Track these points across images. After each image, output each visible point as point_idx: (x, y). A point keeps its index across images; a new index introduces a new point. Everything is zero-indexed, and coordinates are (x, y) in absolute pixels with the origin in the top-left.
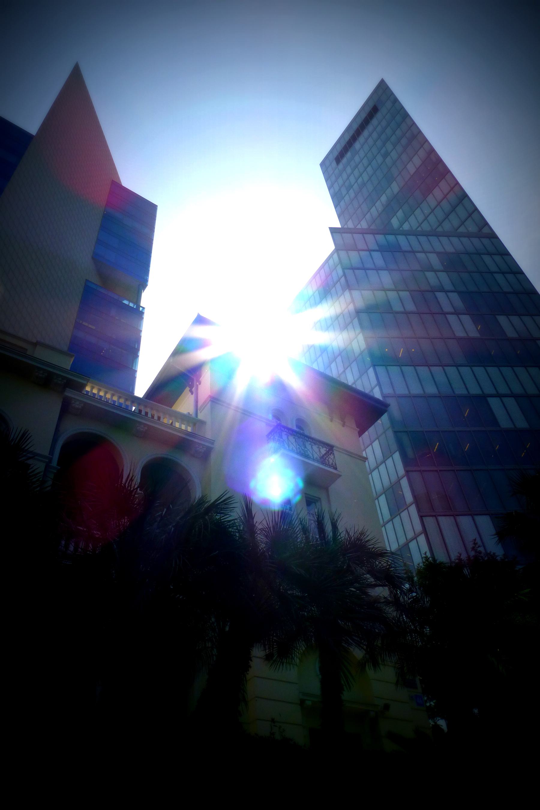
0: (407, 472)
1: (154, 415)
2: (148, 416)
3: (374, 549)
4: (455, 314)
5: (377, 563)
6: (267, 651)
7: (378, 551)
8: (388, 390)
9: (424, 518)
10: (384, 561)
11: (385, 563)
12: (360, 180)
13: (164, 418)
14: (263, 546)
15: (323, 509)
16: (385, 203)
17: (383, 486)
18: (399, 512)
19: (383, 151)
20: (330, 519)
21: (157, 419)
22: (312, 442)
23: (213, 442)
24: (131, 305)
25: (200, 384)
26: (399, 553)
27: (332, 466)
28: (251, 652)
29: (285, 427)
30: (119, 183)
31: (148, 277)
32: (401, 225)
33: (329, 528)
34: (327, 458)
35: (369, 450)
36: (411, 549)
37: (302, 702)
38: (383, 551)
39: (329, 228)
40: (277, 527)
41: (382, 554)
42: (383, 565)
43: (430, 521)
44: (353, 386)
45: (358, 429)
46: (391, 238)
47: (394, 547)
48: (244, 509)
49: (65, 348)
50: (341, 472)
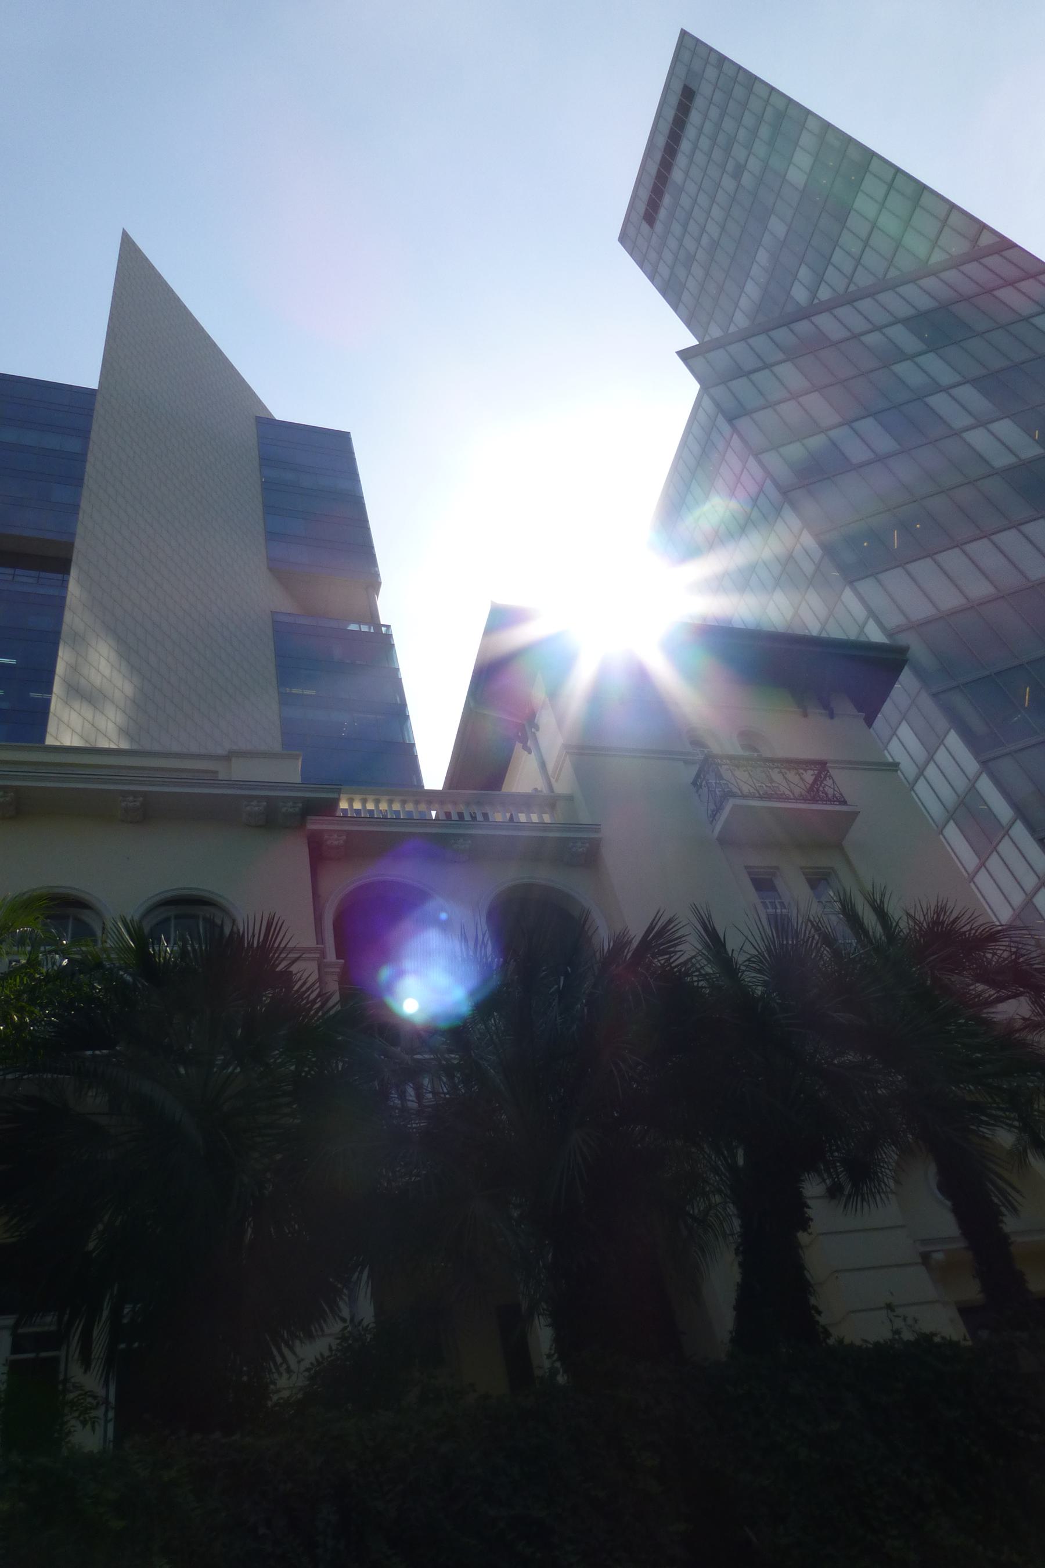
0: (985, 765)
2: (466, 819)
3: (973, 931)
4: (980, 426)
5: (989, 956)
6: (828, 1181)
7: (983, 933)
8: (894, 620)
10: (1001, 948)
11: (1004, 950)
12: (705, 241)
14: (759, 991)
15: (848, 889)
16: (768, 265)
17: (943, 804)
18: (994, 844)
19: (730, 166)
20: (866, 902)
22: (782, 768)
23: (595, 828)
24: (365, 628)
25: (538, 730)
26: (1019, 923)
27: (835, 799)
29: (772, 760)
30: (269, 417)
31: (377, 569)
32: (814, 294)
33: (870, 919)
34: (821, 789)
35: (894, 746)
36: (1040, 909)
37: (926, 1258)
38: (991, 931)
39: (676, 352)
40: (775, 946)
41: (992, 936)
44: (822, 635)
47: (1004, 915)
48: (700, 933)
49: (277, 747)
50: (857, 806)
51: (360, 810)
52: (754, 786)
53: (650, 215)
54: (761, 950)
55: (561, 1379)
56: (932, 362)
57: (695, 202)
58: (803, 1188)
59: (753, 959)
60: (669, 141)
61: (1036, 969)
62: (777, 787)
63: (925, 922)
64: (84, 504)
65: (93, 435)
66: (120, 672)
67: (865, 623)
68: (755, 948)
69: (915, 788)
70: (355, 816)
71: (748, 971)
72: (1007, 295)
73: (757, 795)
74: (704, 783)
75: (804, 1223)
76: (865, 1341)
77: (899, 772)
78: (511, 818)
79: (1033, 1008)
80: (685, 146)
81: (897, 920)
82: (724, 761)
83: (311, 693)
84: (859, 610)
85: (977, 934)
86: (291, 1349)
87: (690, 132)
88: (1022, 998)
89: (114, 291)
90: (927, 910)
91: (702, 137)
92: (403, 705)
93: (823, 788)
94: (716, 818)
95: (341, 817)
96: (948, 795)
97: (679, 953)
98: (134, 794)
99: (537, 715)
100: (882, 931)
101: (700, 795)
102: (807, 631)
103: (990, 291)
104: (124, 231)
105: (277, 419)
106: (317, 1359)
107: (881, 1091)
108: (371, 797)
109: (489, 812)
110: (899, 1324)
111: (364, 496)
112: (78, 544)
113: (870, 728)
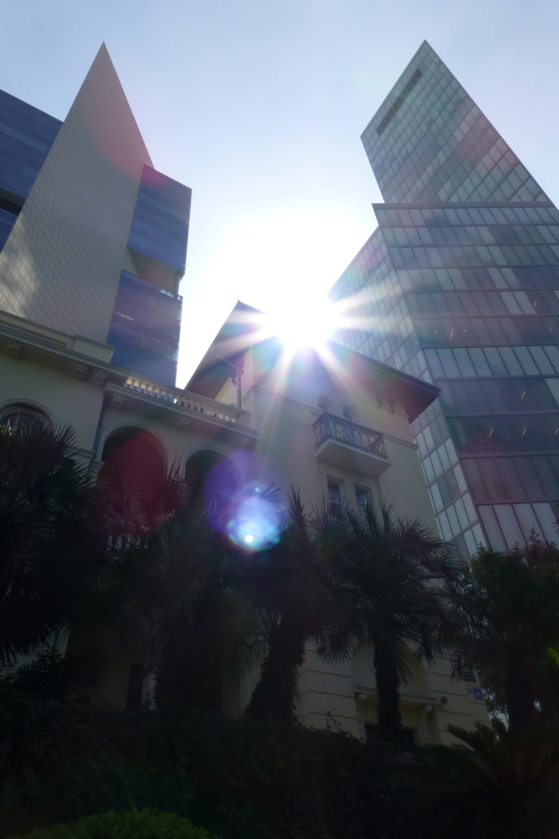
0: (461, 460)
3: (428, 540)
5: (432, 554)
6: (319, 644)
8: (438, 374)
9: (479, 507)
10: (439, 551)
11: (440, 553)
18: (453, 501)
19: (428, 118)
21: (187, 407)
24: (169, 294)
26: (453, 543)
31: (184, 265)
34: (377, 447)
35: (420, 437)
37: (357, 695)
38: (438, 542)
41: (437, 545)
43: (485, 510)
47: (448, 537)
49: (104, 342)
51: (130, 385)
52: (343, 436)
54: (320, 518)
55: (152, 707)
56: (496, 250)
57: (405, 130)
59: (314, 521)
61: (453, 567)
62: (355, 439)
63: (406, 527)
64: (38, 181)
65: (54, 146)
66: (30, 276)
67: (424, 371)
69: (424, 462)
71: (309, 527)
73: (344, 441)
74: (319, 426)
75: (300, 661)
77: (418, 450)
79: (446, 585)
83: (130, 319)
84: (423, 364)
85: (430, 541)
86: (14, 656)
88: (441, 579)
89: (88, 73)
90: (410, 522)
93: (378, 447)
94: (320, 446)
95: (133, 390)
98: (18, 342)
100: (383, 525)
101: (315, 432)
104: (104, 41)
105: (155, 170)
106: (24, 666)
107: (360, 606)
108: (145, 382)
110: (331, 723)
111: (190, 225)
112: (28, 201)
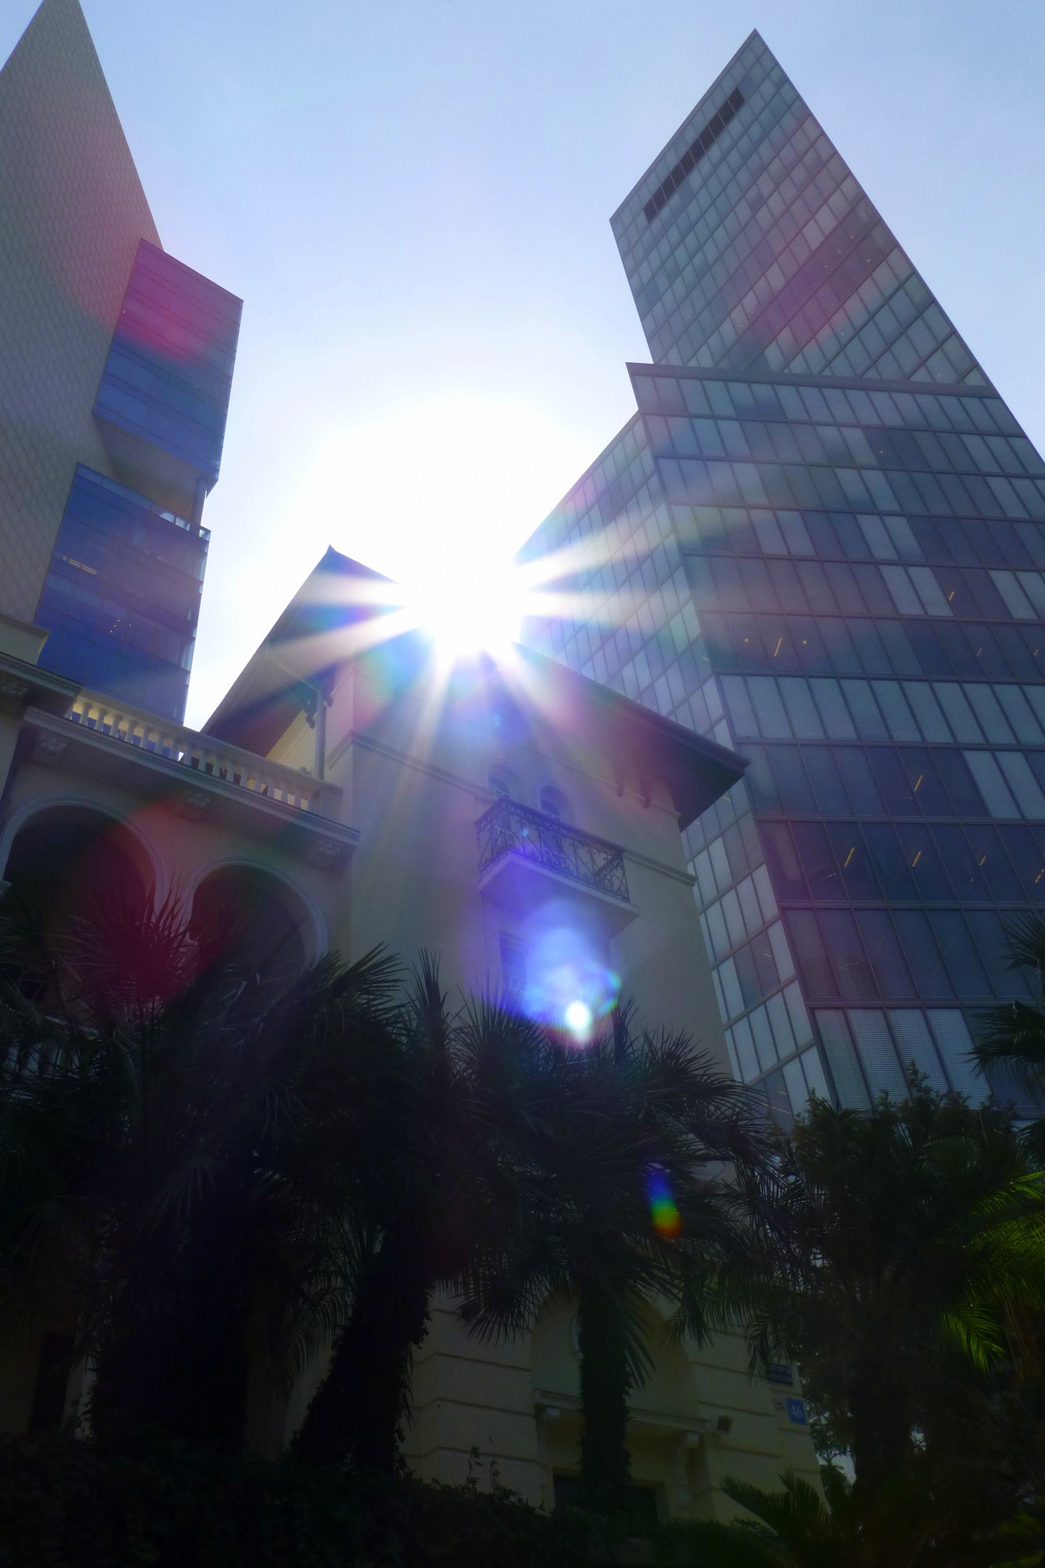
1: (226, 771)
5: (712, 1108)
7: (716, 1082)
8: (747, 729)
9: (817, 1012)
11: (729, 1108)
12: (698, 259)
13: (248, 779)
19: (752, 193)
21: (204, 771)
24: (180, 523)
25: (330, 704)
27: (619, 893)
28: (430, 1299)
32: (788, 361)
34: (609, 877)
35: (702, 859)
37: (539, 1411)
38: (724, 1083)
39: (626, 363)
41: (722, 1089)
42: (725, 1113)
43: (829, 1019)
45: (677, 813)
46: (764, 391)
47: (751, 1075)
49: (28, 617)
53: (651, 210)
58: (430, 1295)
59: (466, 1030)
60: (700, 140)
68: (471, 1017)
70: (87, 725)
71: (455, 1041)
72: (973, 442)
74: (488, 827)
75: (418, 1334)
76: (437, 1482)
78: (265, 792)
80: (714, 152)
81: (632, 1040)
82: (588, 841)
84: (716, 708)
87: (725, 140)
91: (735, 151)
92: (193, 624)
96: (737, 932)
97: (385, 997)
99: (335, 689)
101: (479, 838)
102: (656, 708)
103: (958, 433)
105: (166, 250)
109: (242, 775)
113: (681, 830)
